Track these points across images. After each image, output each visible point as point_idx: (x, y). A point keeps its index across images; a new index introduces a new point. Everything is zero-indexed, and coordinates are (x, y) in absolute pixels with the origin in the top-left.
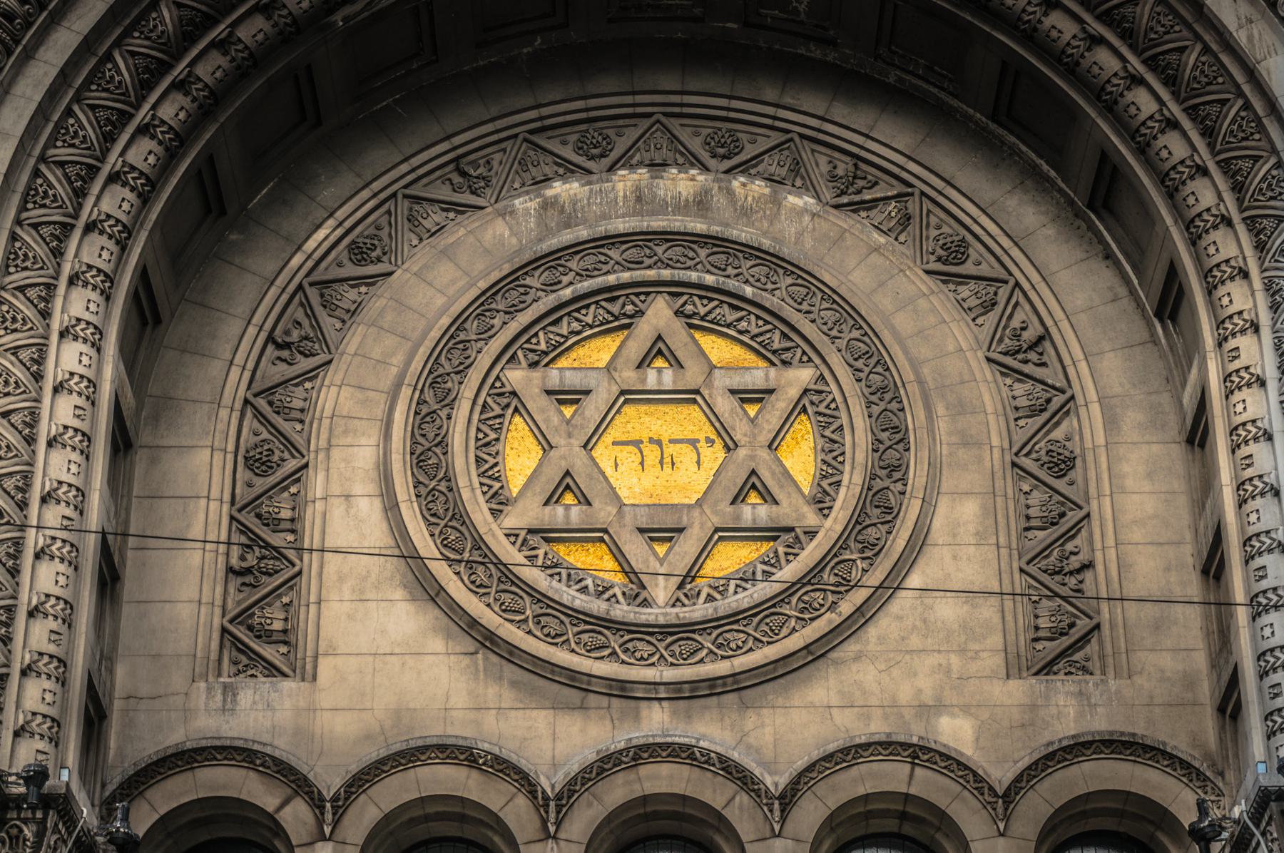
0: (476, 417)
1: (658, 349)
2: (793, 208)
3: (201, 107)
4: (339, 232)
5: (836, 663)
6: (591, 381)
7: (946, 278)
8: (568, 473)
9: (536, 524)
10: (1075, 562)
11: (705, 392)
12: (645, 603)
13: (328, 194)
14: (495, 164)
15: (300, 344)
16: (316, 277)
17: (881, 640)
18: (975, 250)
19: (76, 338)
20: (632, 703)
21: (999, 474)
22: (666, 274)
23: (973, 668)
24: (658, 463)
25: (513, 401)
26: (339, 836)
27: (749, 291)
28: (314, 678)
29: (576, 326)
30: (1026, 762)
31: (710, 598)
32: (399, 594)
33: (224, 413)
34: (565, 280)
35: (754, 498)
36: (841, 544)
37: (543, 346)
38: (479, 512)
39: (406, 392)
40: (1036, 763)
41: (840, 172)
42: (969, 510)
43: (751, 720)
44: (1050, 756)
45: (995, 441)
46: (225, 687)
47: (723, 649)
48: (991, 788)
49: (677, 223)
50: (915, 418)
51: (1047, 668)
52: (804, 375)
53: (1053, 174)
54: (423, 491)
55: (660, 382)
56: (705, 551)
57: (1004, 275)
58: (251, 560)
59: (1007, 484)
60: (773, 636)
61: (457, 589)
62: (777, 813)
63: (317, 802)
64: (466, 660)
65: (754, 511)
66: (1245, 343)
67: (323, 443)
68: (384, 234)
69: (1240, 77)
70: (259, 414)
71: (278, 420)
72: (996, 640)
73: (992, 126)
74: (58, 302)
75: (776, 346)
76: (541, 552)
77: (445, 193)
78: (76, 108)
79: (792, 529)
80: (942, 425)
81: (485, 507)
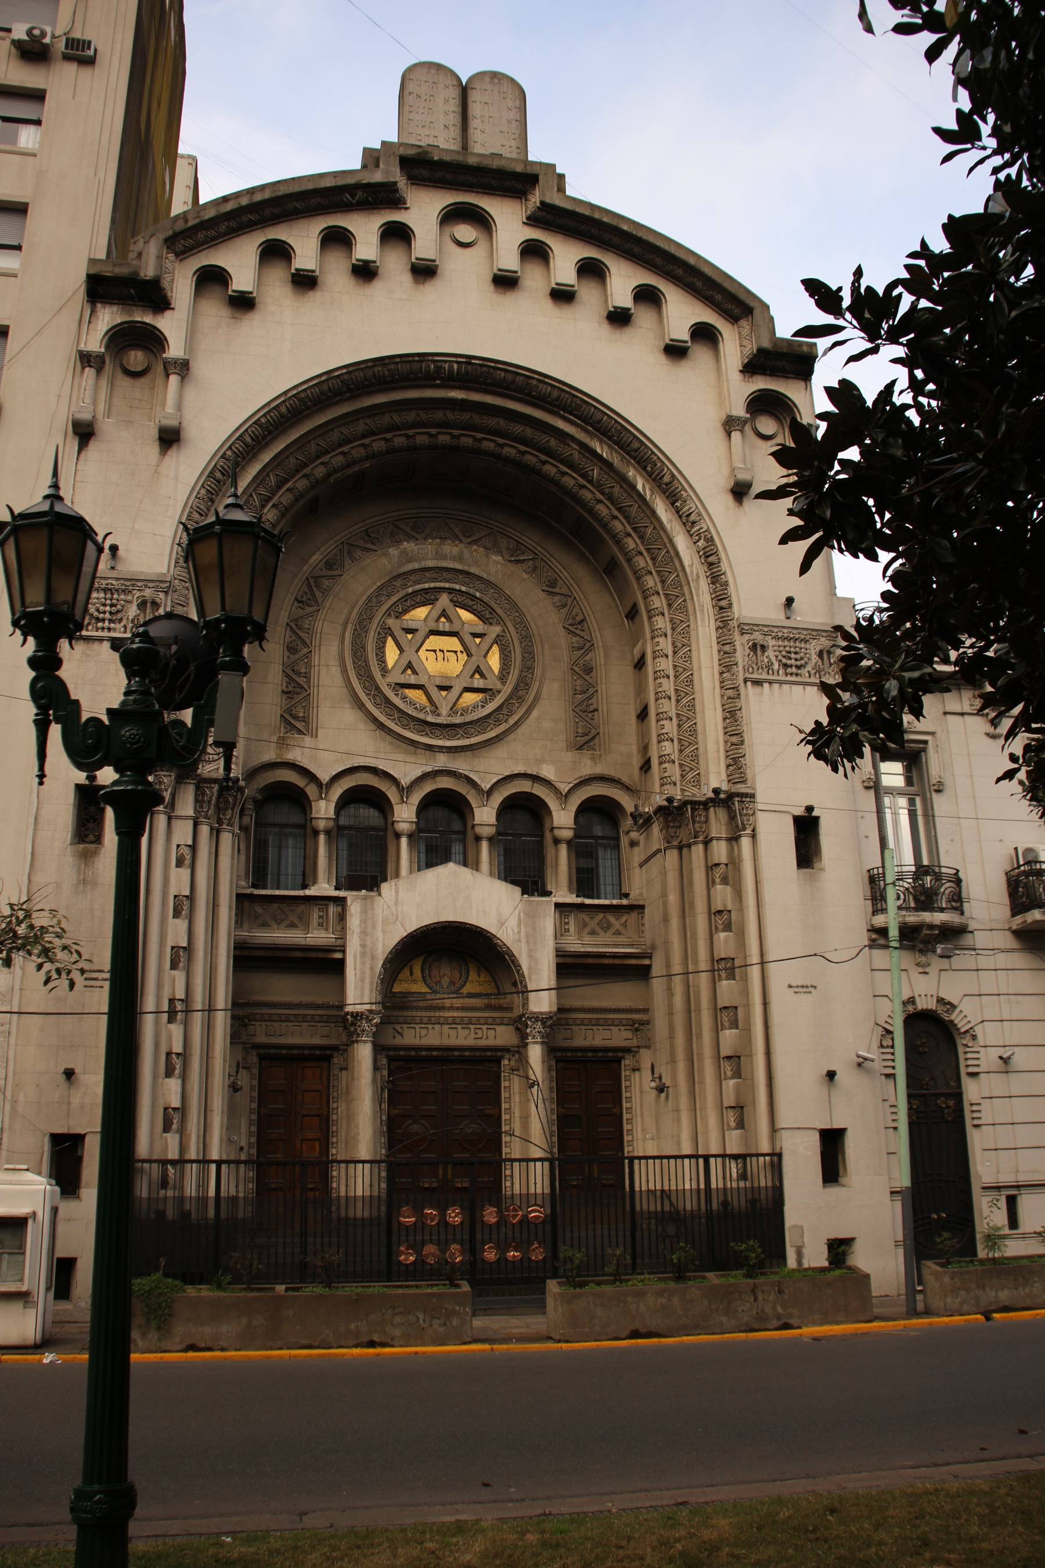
1: (444, 614)
2: (494, 561)
10: (591, 708)
12: (438, 715)
18: (560, 583)
22: (447, 585)
24: (441, 660)
31: (462, 715)
32: (347, 706)
39: (350, 626)
42: (556, 686)
49: (451, 565)
50: (537, 649)
51: (581, 748)
58: (290, 689)
66: (661, 640)
68: (338, 558)
69: (666, 541)
71: (298, 631)
72: (563, 737)
73: (569, 536)
77: (361, 543)
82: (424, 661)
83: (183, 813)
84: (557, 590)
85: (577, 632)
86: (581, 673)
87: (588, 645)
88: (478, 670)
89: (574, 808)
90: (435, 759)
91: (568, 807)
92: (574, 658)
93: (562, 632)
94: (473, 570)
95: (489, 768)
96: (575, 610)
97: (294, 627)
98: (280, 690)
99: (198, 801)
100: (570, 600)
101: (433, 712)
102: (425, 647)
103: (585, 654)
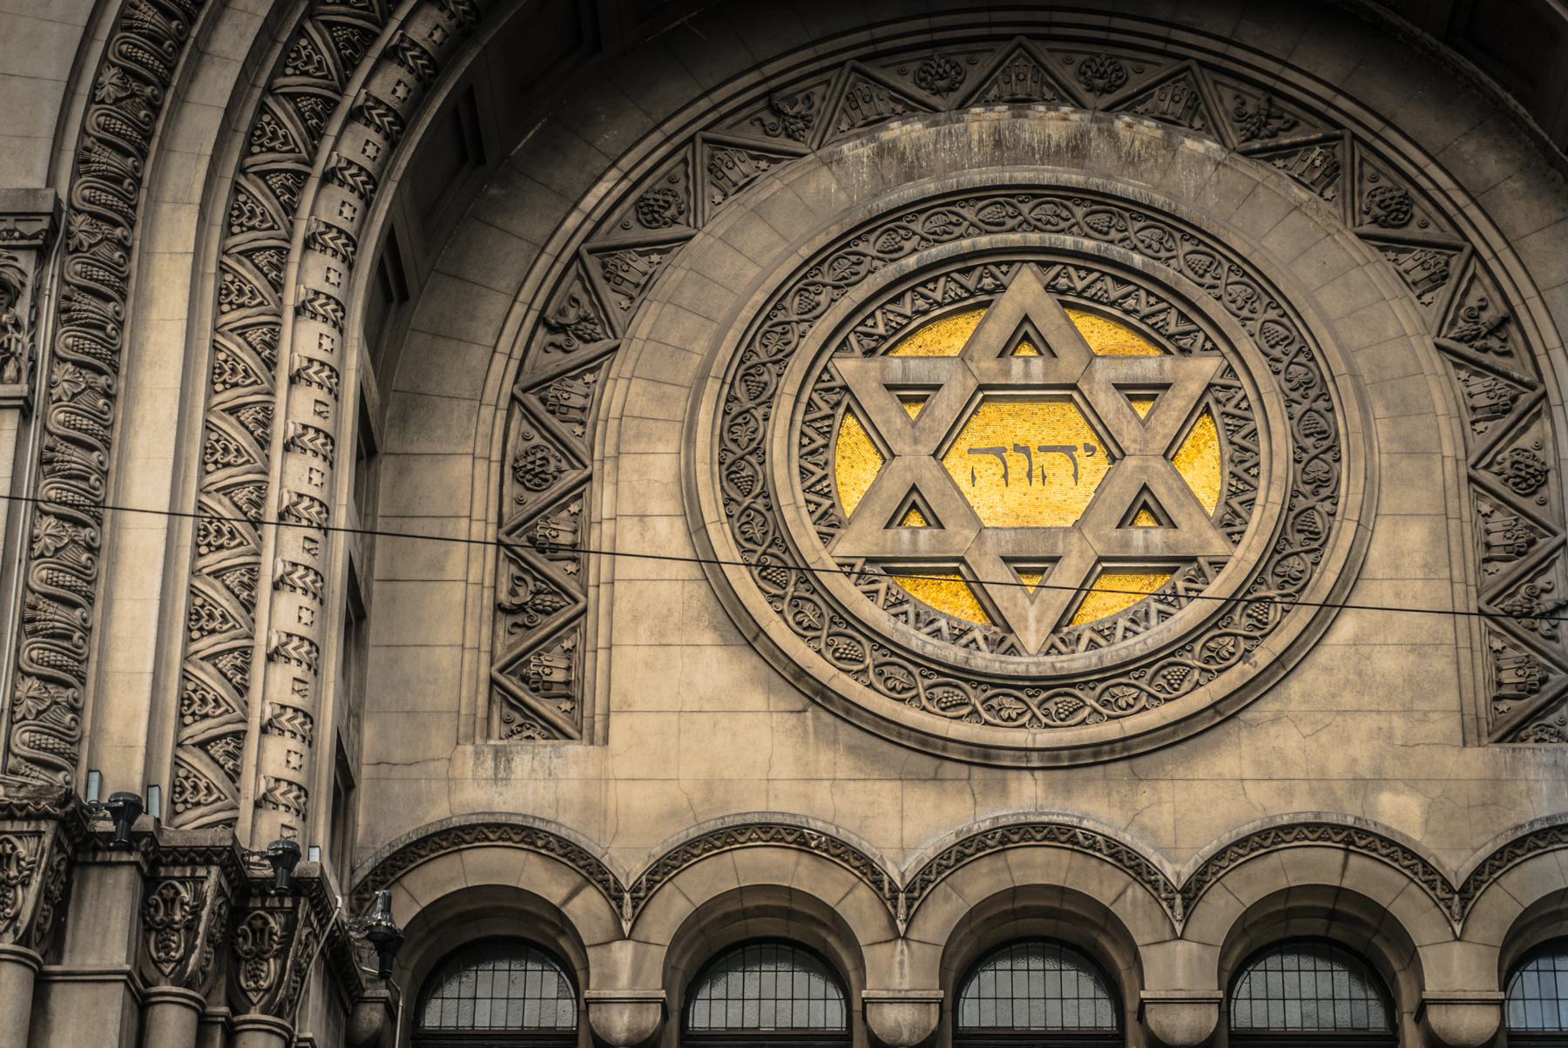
0: (799, 417)
1: (1025, 333)
2: (1192, 154)
3: (460, 25)
4: (625, 185)
5: (1249, 725)
6: (941, 373)
7: (1385, 244)
8: (914, 488)
9: (875, 552)
10: (1547, 602)
11: (1084, 388)
12: (1012, 650)
13: (609, 138)
14: (817, 100)
15: (579, 327)
16: (596, 242)
17: (1306, 697)
18: (1421, 208)
19: (314, 316)
20: (998, 774)
21: (1452, 491)
22: (1034, 238)
23: (1422, 732)
25: (844, 398)
26: (640, 933)
27: (1137, 260)
28: (606, 741)
29: (921, 304)
30: (1489, 849)
31: (1093, 645)
32: (708, 637)
33: (487, 412)
34: (908, 246)
35: (1144, 520)
36: (1257, 577)
37: (881, 330)
38: (806, 536)
39: (712, 386)
40: (1501, 851)
41: (1250, 109)
42: (1416, 535)
43: (1144, 795)
44: (1518, 843)
45: (1448, 450)
46: (497, 752)
47: (1111, 708)
48: (1445, 882)
49: (1046, 174)
50: (1348, 420)
51: (1513, 734)
52: (1207, 367)
53: (1522, 110)
54: (736, 510)
55: (1027, 374)
56: (1084, 589)
57: (1458, 241)
58: (524, 595)
59: (1462, 504)
60: (1172, 691)
61: (780, 633)
62: (1179, 910)
63: (613, 893)
64: (792, 720)
65: (1146, 537)
67: (610, 450)
68: (679, 188)
70: (529, 414)
71: (553, 422)
72: (1450, 699)
73: (1445, 50)
74: (292, 272)
75: (1172, 329)
76: (882, 587)
77: (754, 136)
78: (309, 26)
79: (1193, 559)
80: (1381, 430)
81: (812, 530)
82: (965, 486)
83: (91, 963)
84: (1413, 231)
85: (1487, 358)
86: (1506, 491)
87: (1525, 399)
88: (1144, 504)
89: (1497, 935)
90: (1004, 791)
91: (1477, 930)
92: (1478, 445)
93: (1437, 364)
94: (1119, 187)
95: (1185, 812)
96: (1476, 294)
97: (539, 408)
98: (488, 601)
99: (150, 924)
100: (1456, 263)
101: (996, 644)
102: (968, 439)
103: (1519, 427)
